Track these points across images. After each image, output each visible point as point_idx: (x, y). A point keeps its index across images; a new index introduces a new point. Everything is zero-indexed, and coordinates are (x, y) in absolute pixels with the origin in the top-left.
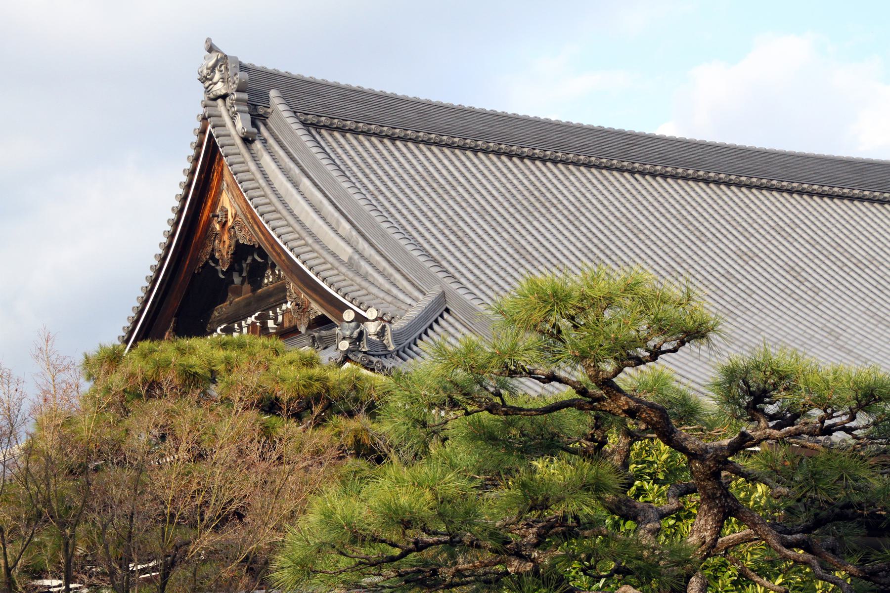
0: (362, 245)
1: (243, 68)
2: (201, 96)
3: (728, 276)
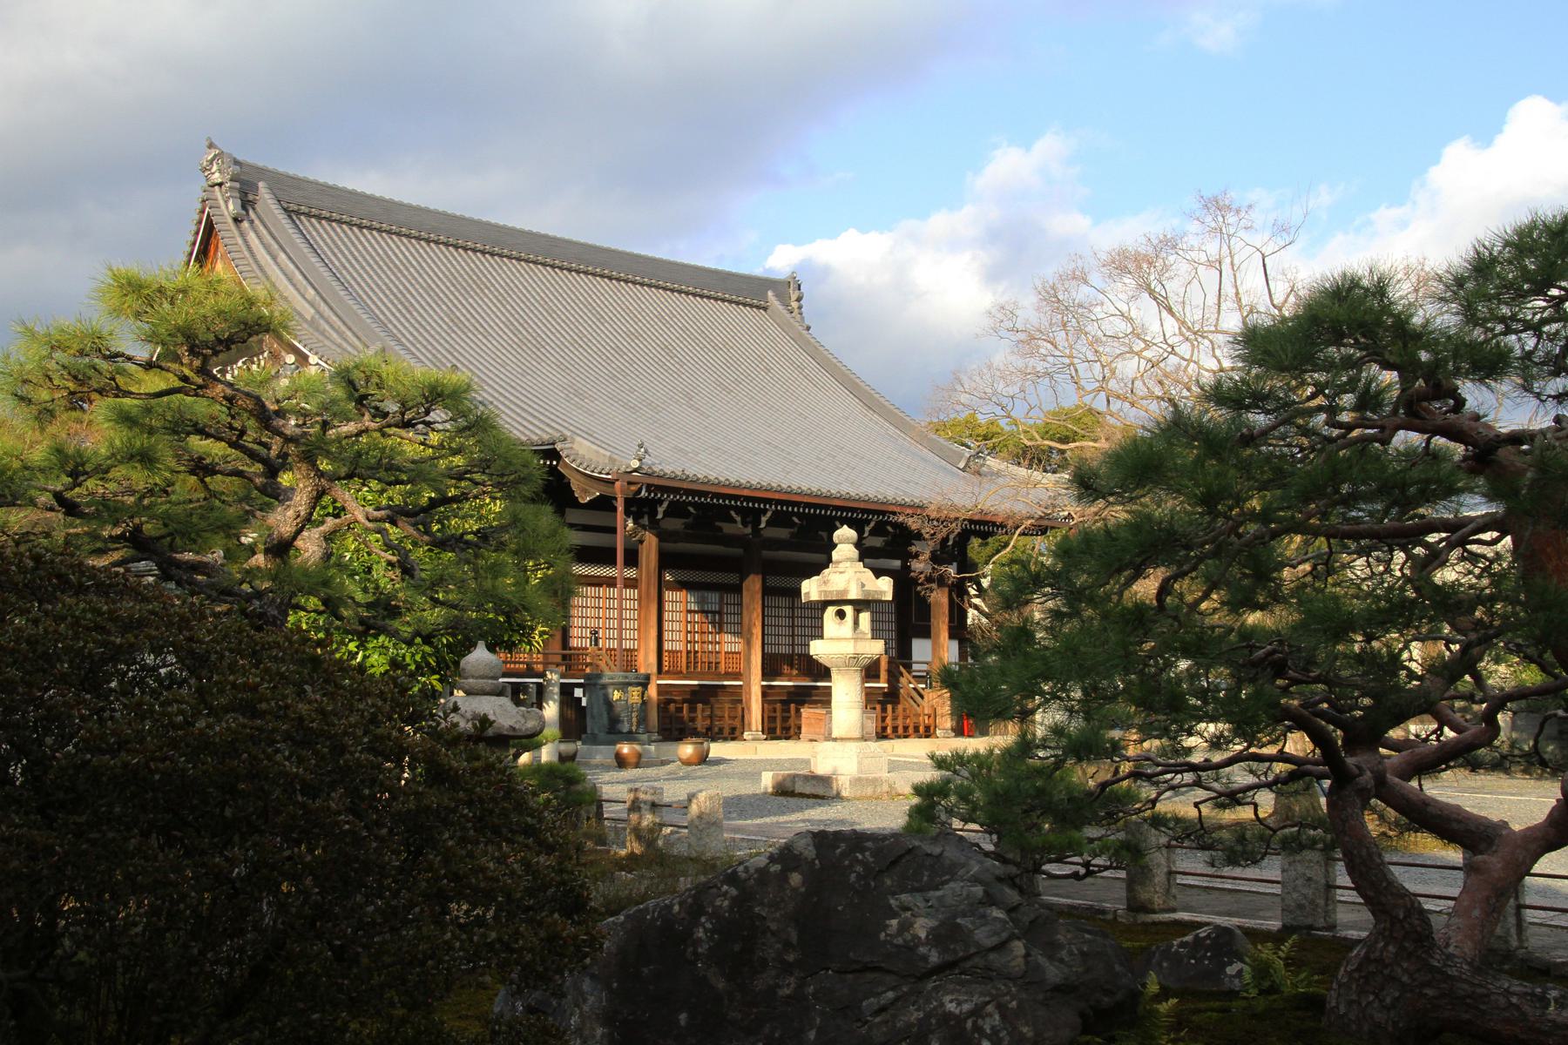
1: (236, 162)
3: (617, 350)
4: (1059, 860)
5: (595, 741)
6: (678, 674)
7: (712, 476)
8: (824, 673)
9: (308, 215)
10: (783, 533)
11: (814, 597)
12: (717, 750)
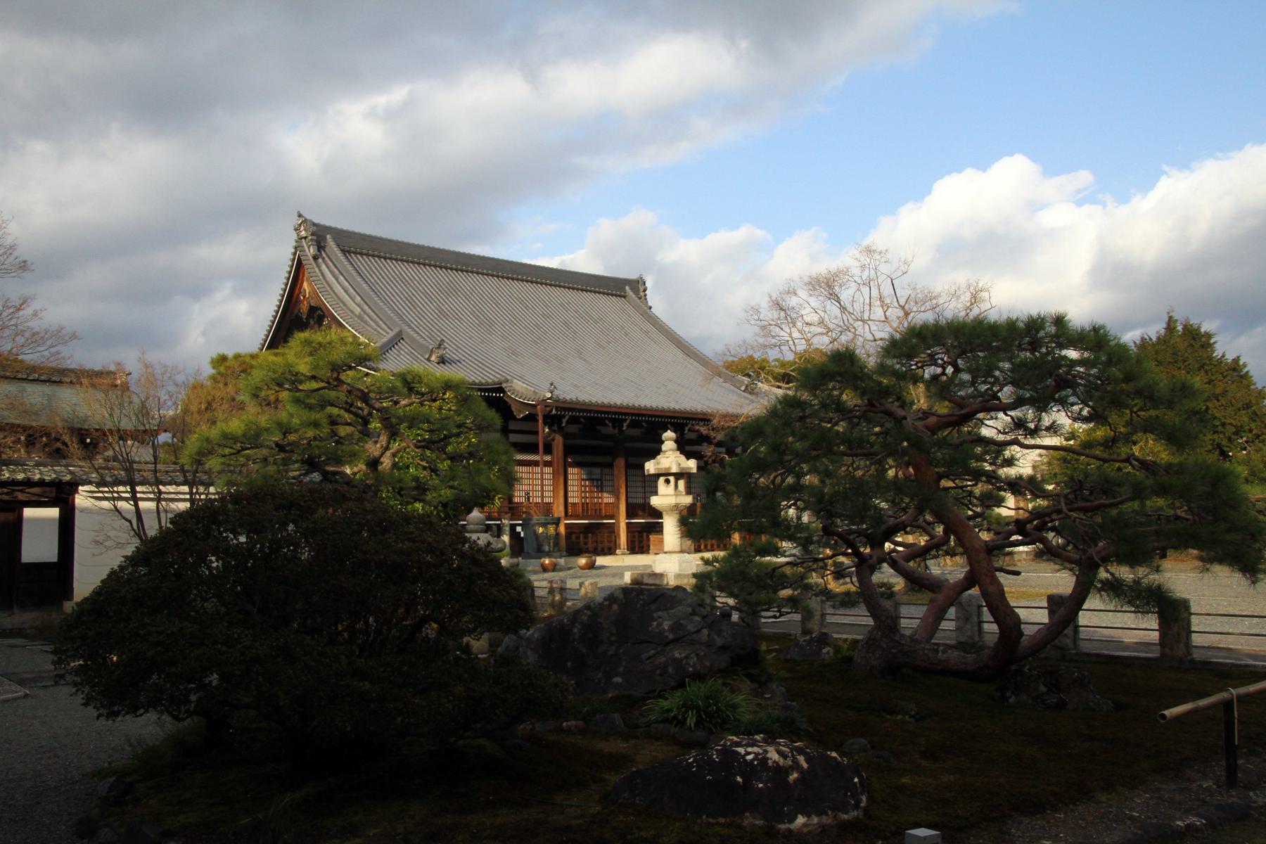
0: (366, 307)
1: (314, 224)
2: (295, 237)
3: (537, 325)
4: (767, 610)
5: (529, 556)
6: (578, 518)
7: (594, 400)
8: (658, 514)
9: (355, 253)
10: (636, 432)
11: (652, 472)
12: (600, 561)
